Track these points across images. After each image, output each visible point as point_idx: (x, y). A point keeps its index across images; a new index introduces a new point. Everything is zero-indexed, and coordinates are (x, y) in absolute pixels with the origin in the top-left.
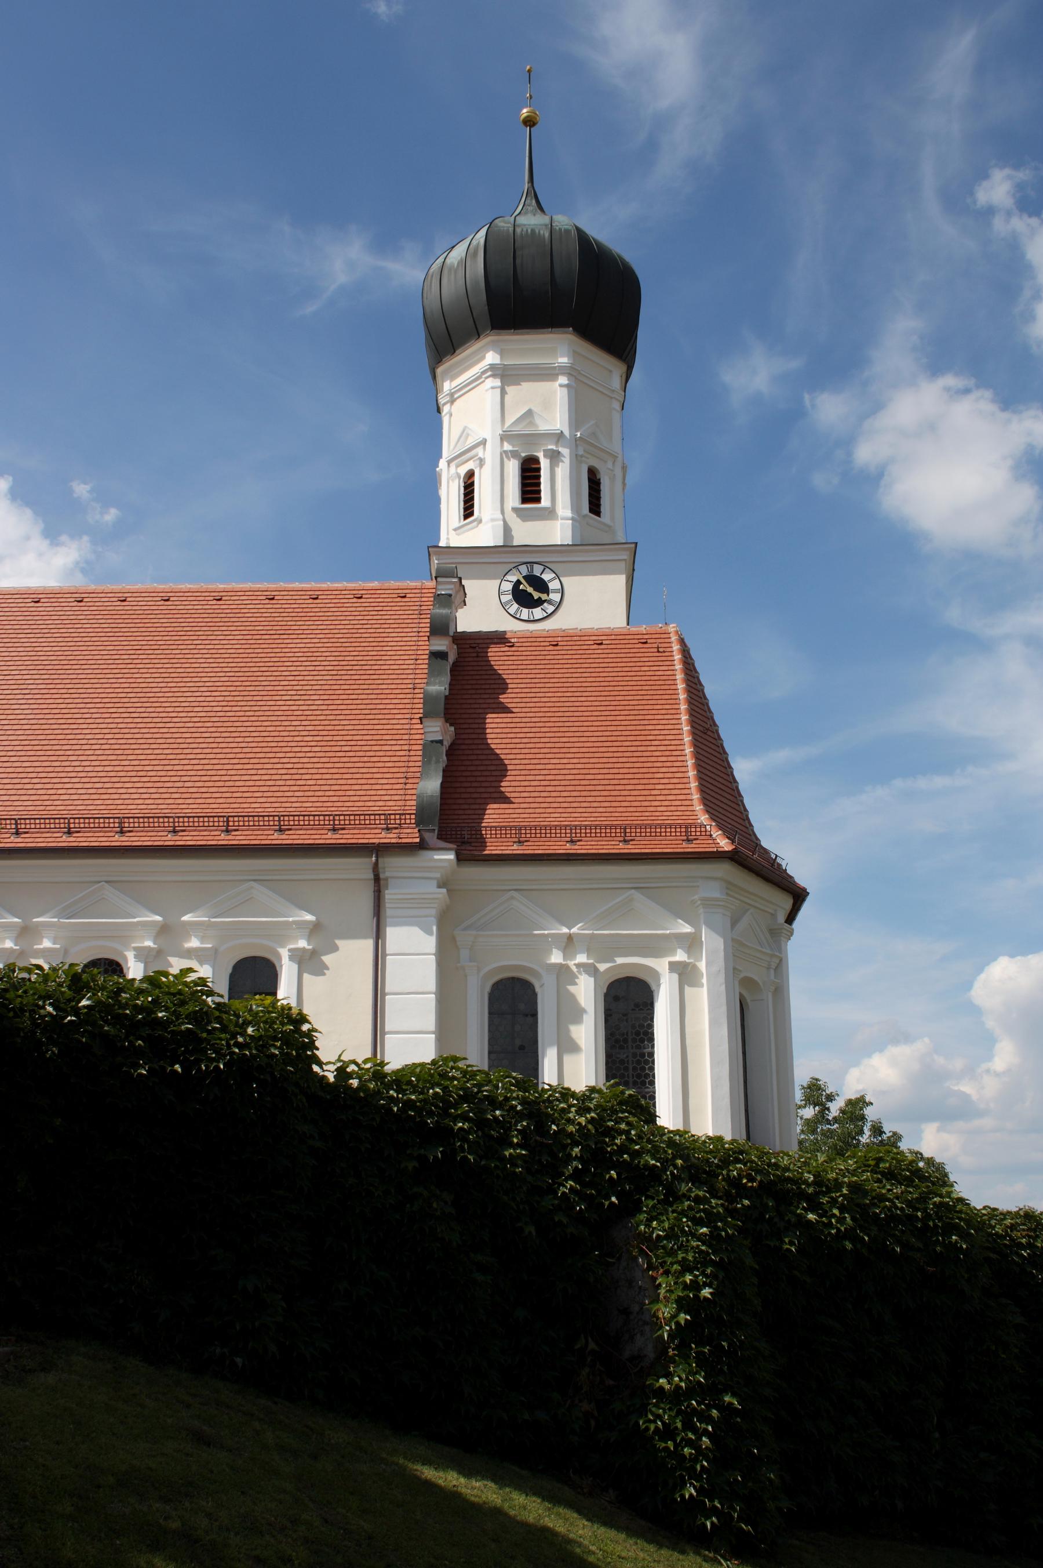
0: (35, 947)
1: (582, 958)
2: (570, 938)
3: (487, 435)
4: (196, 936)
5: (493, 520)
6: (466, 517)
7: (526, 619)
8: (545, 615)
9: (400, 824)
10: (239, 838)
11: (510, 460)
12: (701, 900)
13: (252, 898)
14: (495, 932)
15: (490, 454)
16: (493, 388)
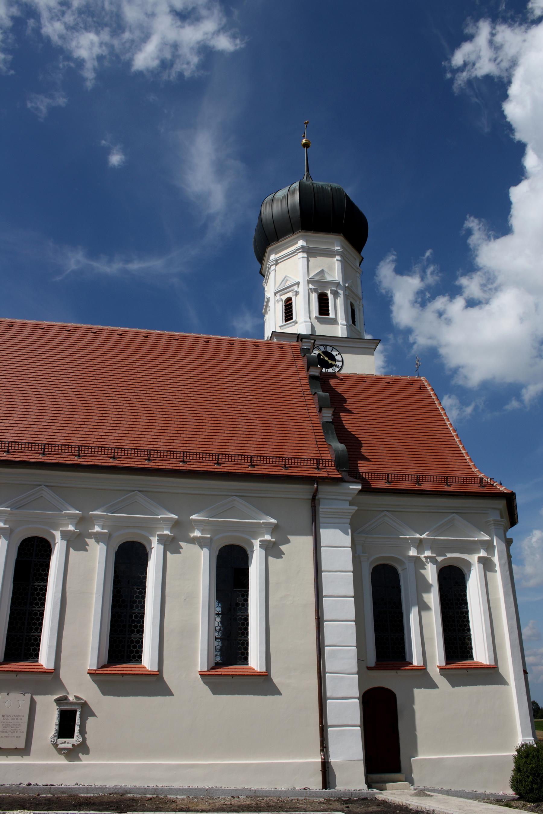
0: (90, 531)
1: (428, 553)
2: (421, 540)
3: (300, 280)
4: (198, 530)
5: (305, 322)
9: (325, 466)
10: (226, 468)
11: (313, 293)
12: (493, 521)
13: (234, 507)
14: (375, 536)
15: (302, 289)
16: (303, 257)
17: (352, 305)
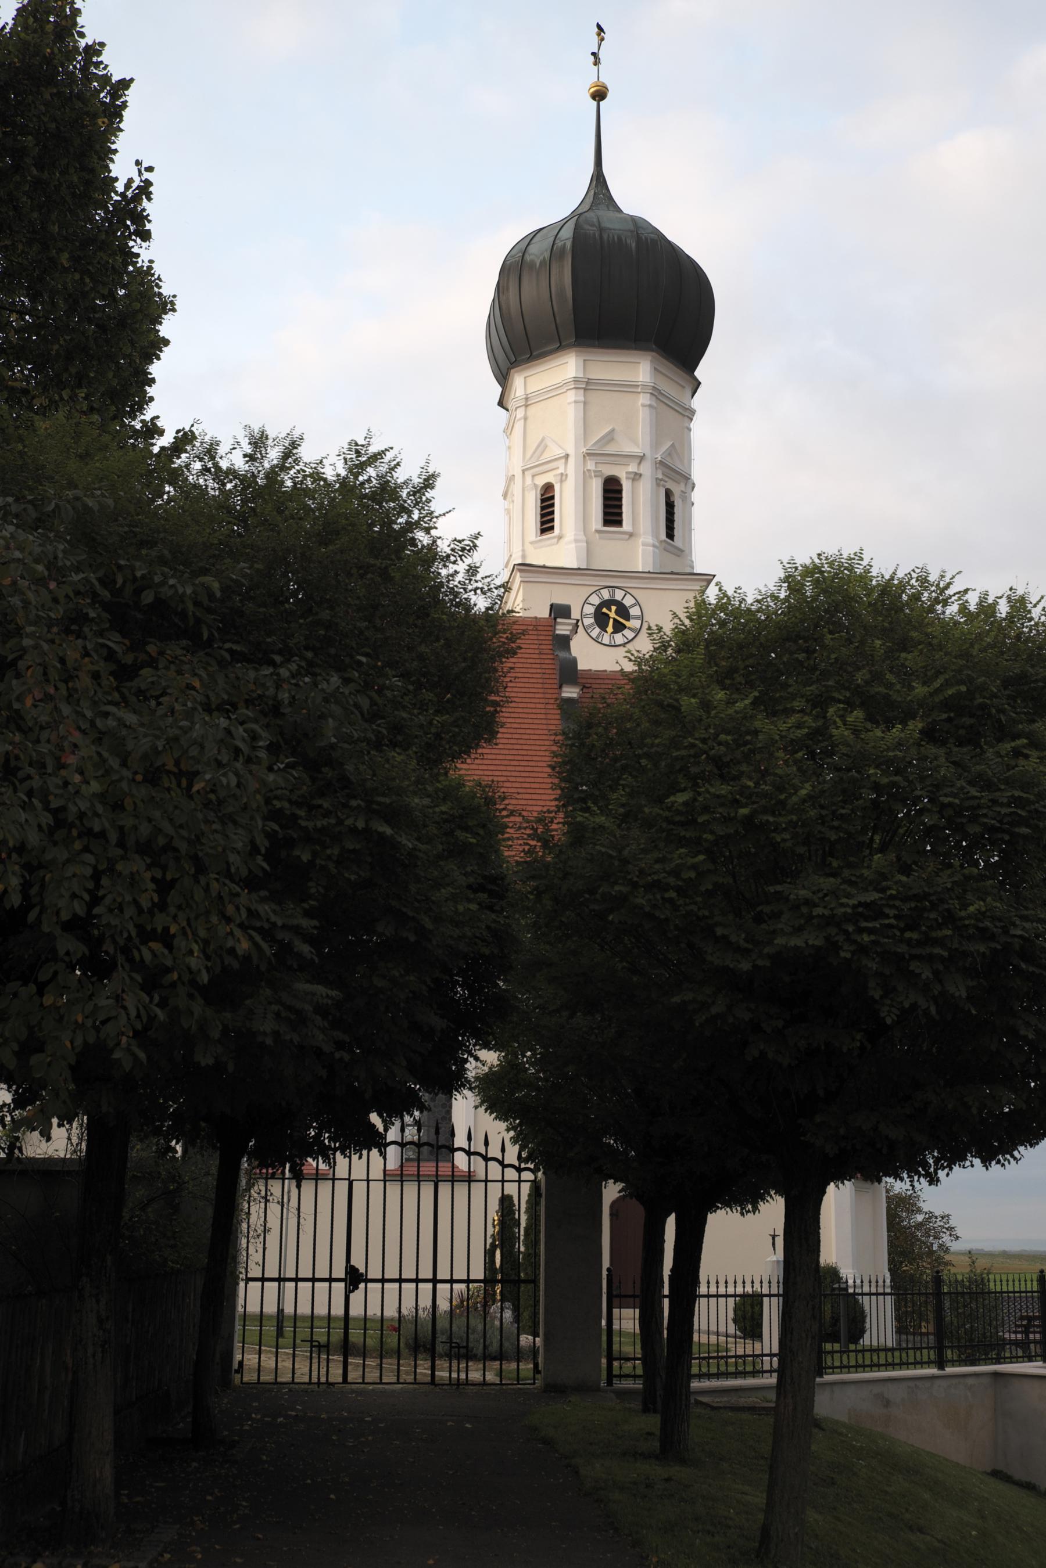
6: (543, 531)
7: (608, 643)
8: (626, 641)
17: (668, 494)
